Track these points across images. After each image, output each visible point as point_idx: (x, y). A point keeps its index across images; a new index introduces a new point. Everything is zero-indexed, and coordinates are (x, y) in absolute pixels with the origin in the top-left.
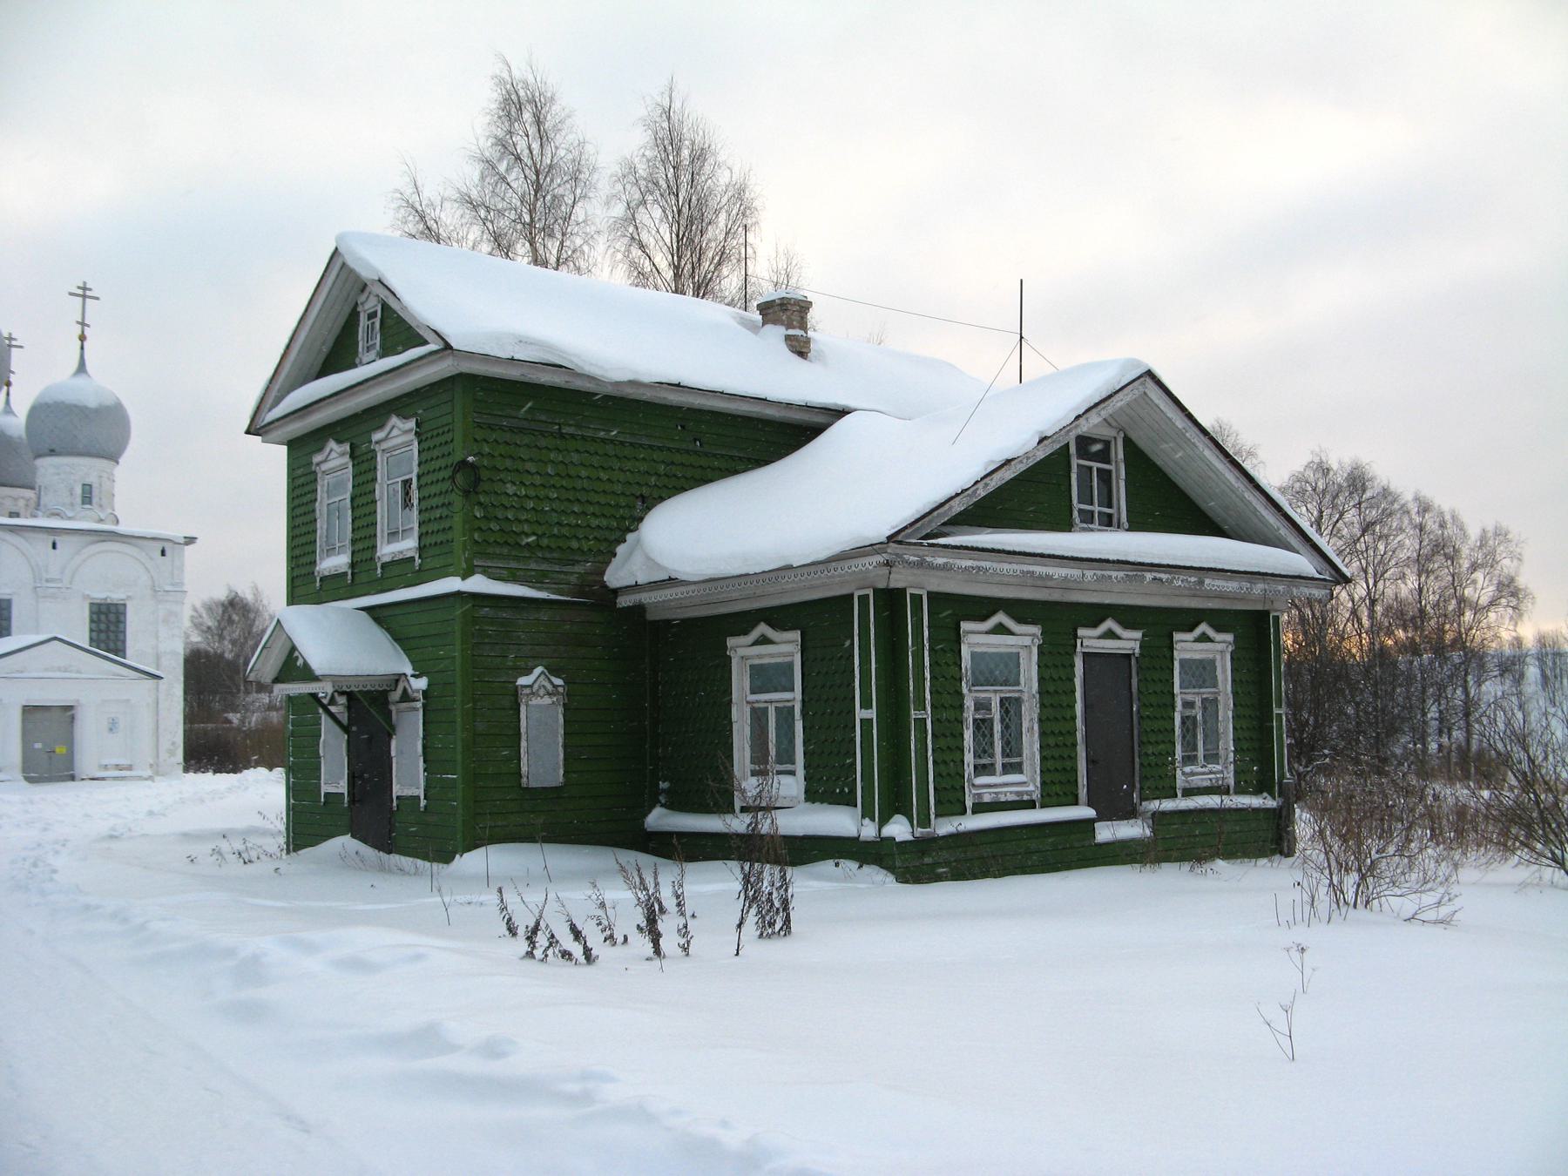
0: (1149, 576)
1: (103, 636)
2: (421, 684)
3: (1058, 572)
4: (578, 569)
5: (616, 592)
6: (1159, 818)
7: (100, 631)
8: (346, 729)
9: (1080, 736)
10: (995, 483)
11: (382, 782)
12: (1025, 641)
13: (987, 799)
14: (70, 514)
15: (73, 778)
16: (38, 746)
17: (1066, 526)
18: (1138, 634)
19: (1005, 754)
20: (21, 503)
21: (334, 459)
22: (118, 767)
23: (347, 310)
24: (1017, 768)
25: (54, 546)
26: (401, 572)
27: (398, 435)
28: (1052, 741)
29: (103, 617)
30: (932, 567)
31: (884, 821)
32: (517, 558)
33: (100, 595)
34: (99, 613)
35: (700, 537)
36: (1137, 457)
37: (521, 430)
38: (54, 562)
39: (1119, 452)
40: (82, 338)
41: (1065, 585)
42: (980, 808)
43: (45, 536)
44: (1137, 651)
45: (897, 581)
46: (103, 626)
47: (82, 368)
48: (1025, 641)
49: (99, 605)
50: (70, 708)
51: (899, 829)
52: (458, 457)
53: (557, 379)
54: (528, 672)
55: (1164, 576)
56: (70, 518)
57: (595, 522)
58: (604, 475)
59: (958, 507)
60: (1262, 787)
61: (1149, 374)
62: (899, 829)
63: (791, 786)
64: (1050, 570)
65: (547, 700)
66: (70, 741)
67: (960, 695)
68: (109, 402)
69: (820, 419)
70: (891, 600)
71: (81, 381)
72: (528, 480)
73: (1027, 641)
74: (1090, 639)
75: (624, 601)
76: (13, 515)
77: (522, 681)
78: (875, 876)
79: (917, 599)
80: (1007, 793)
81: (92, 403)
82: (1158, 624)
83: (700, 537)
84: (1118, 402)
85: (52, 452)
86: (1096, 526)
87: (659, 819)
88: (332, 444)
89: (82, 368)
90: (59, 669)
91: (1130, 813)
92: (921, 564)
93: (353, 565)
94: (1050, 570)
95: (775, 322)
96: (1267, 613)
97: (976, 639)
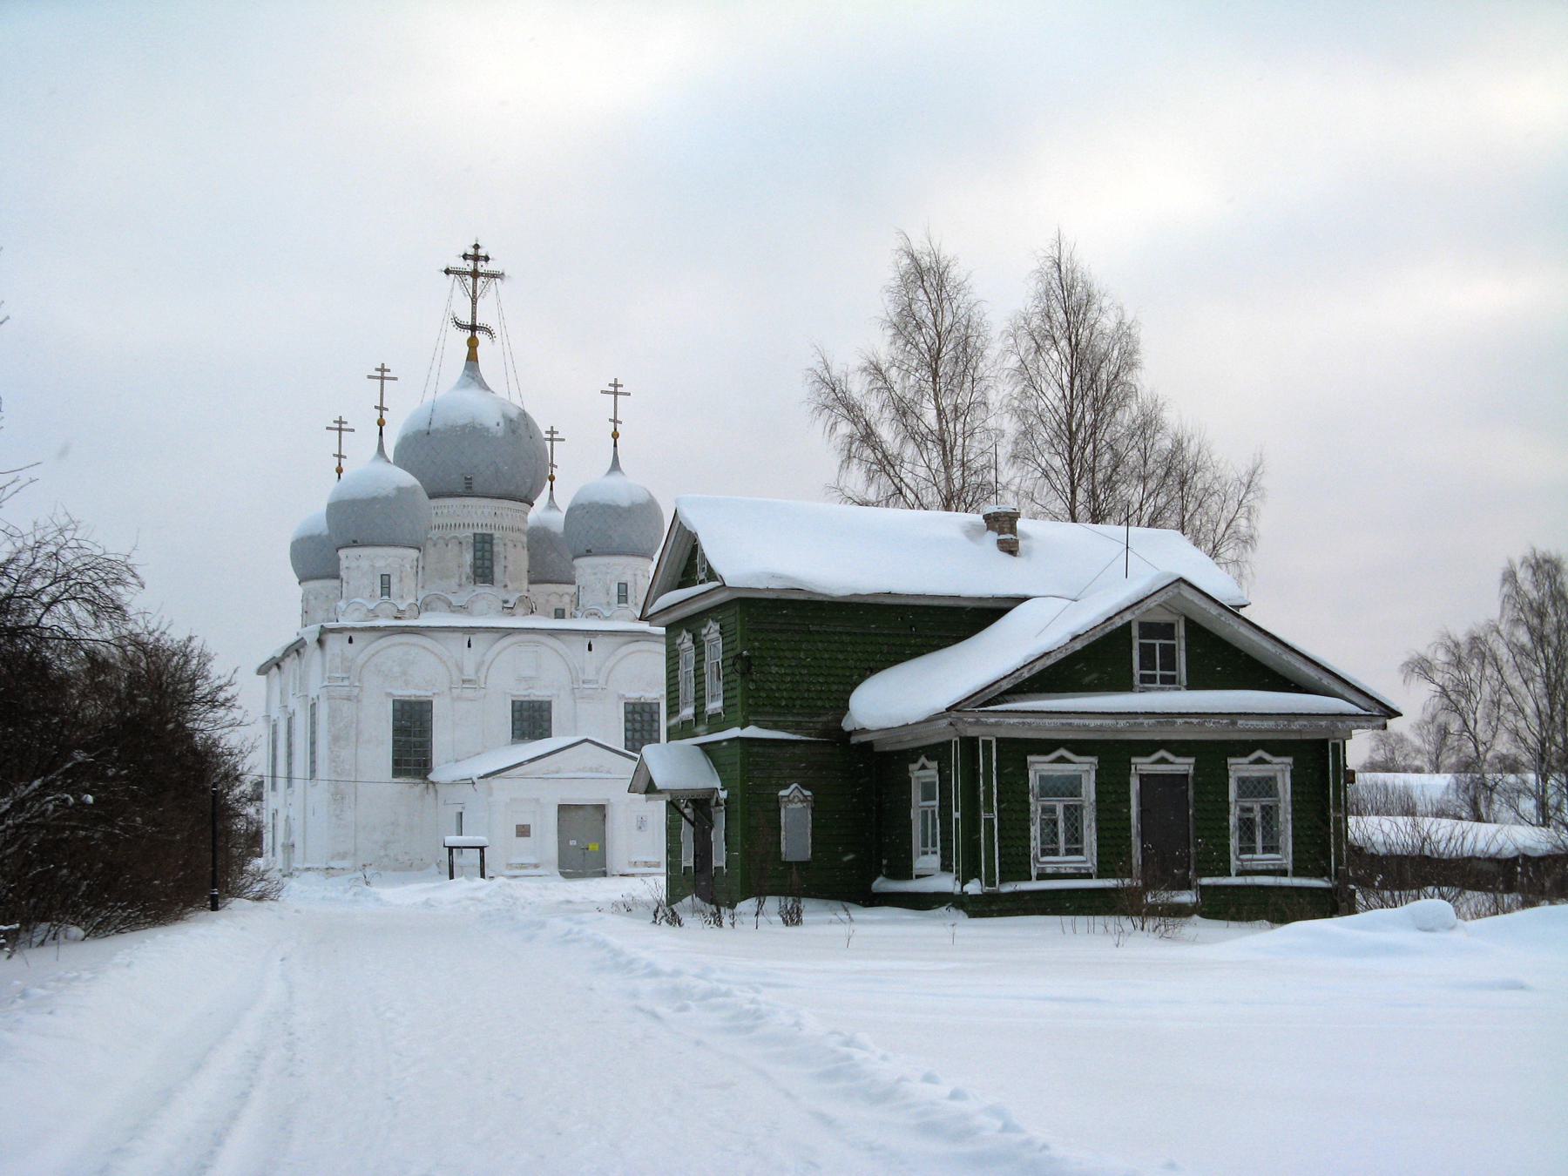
0: (1179, 721)
1: (637, 735)
2: (723, 795)
3: (1093, 722)
4: (824, 719)
5: (850, 733)
6: (1204, 889)
7: (634, 730)
8: (693, 824)
9: (1134, 831)
10: (1038, 667)
11: (731, 860)
12: (1085, 768)
13: (1049, 871)
14: (607, 614)
15: (605, 874)
16: (573, 843)
17: (1125, 686)
18: (1192, 760)
19: (1067, 841)
20: (567, 599)
21: (685, 641)
22: (646, 864)
23: (689, 547)
24: (1079, 852)
25: (590, 648)
26: (716, 723)
27: (712, 631)
28: (1107, 834)
29: (638, 717)
30: (987, 724)
31: (964, 883)
32: (780, 715)
33: (633, 695)
34: (633, 712)
35: (892, 700)
36: (1196, 631)
37: (781, 631)
38: (590, 663)
39: (1181, 631)
40: (615, 435)
41: (1099, 729)
42: (1042, 876)
43: (459, 635)
44: (1191, 771)
45: (971, 732)
46: (638, 726)
47: (615, 465)
48: (1085, 768)
49: (634, 704)
50: (603, 807)
51: (974, 887)
52: (738, 651)
53: (802, 597)
54: (787, 787)
55: (1195, 721)
56: (607, 618)
57: (834, 687)
58: (841, 656)
59: (1006, 685)
60: (1322, 873)
61: (1181, 580)
62: (974, 887)
63: (934, 861)
64: (1087, 722)
65: (800, 805)
66: (602, 838)
67: (1028, 804)
68: (641, 498)
69: (1005, 605)
70: (970, 744)
71: (615, 479)
72: (786, 663)
73: (1086, 767)
74: (1143, 765)
75: (854, 740)
76: (560, 614)
77: (782, 793)
78: (960, 917)
79: (987, 744)
80: (1077, 866)
81: (625, 502)
82: (1213, 754)
83: (892, 700)
84: (1151, 603)
85: (589, 553)
86: (1158, 685)
87: (882, 885)
88: (711, 623)
89: (615, 465)
90: (591, 770)
91: (1186, 885)
92: (978, 723)
93: (696, 715)
94: (1087, 722)
95: (993, 529)
96: (1326, 741)
97: (1040, 768)
